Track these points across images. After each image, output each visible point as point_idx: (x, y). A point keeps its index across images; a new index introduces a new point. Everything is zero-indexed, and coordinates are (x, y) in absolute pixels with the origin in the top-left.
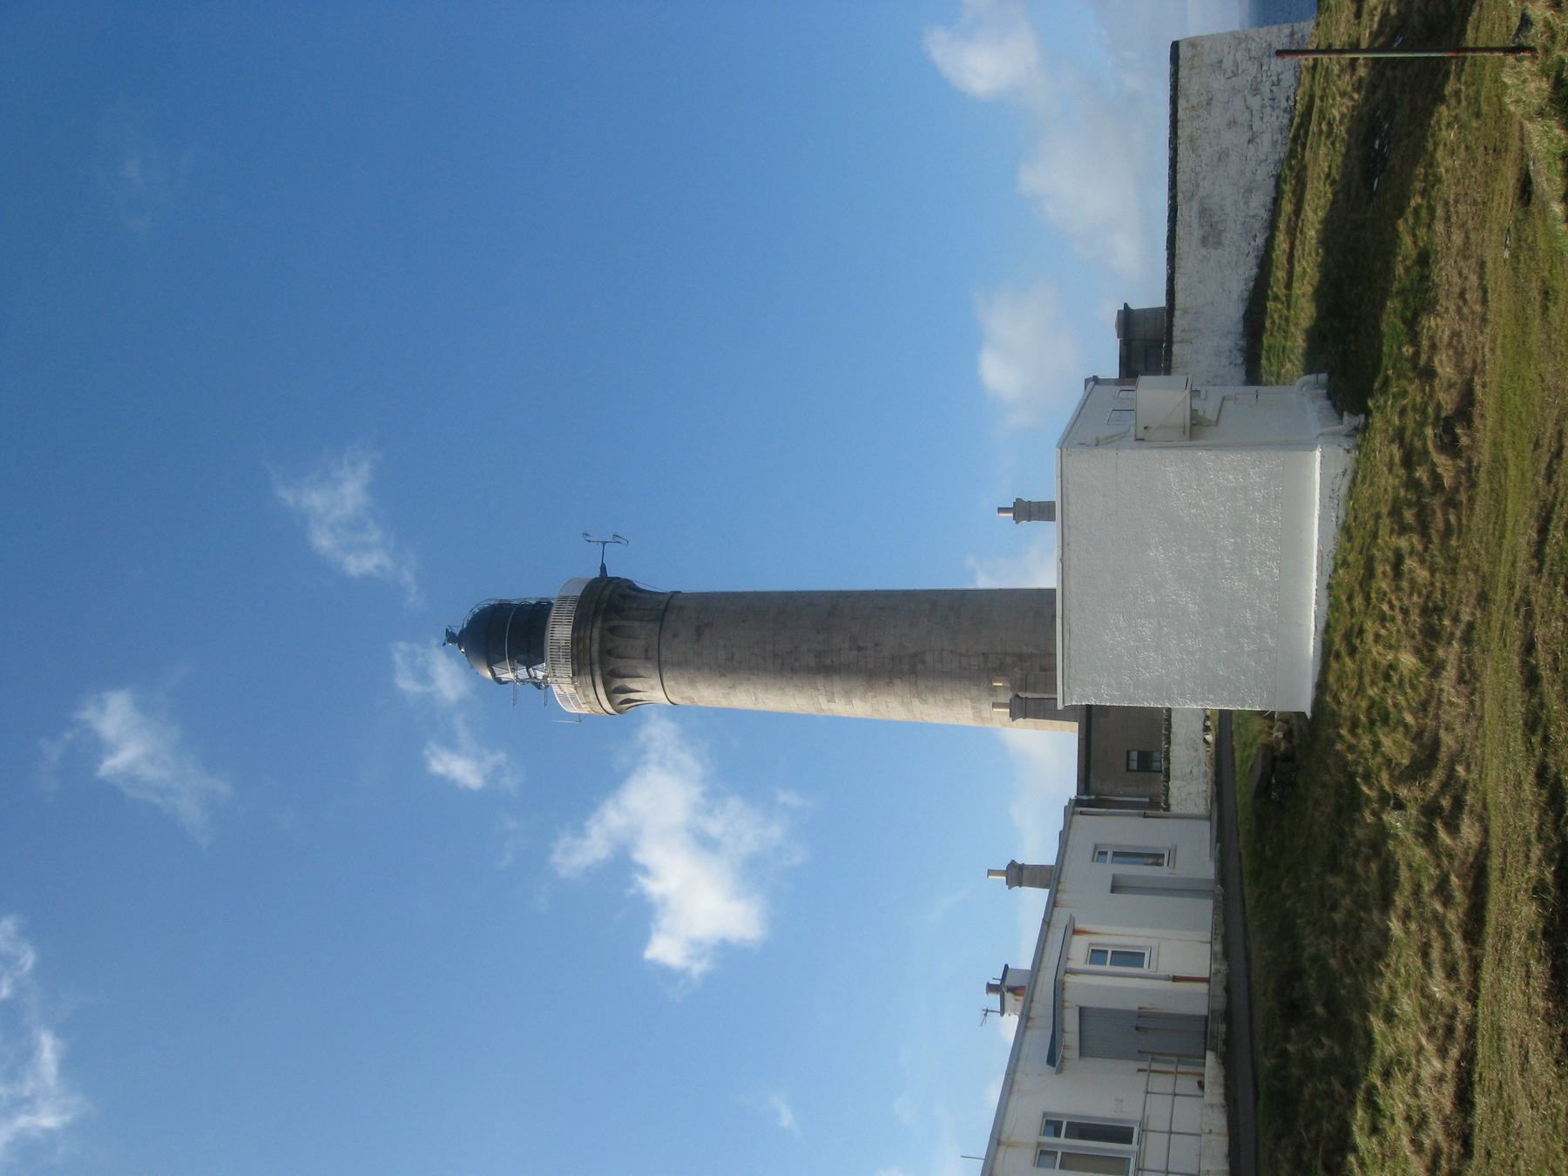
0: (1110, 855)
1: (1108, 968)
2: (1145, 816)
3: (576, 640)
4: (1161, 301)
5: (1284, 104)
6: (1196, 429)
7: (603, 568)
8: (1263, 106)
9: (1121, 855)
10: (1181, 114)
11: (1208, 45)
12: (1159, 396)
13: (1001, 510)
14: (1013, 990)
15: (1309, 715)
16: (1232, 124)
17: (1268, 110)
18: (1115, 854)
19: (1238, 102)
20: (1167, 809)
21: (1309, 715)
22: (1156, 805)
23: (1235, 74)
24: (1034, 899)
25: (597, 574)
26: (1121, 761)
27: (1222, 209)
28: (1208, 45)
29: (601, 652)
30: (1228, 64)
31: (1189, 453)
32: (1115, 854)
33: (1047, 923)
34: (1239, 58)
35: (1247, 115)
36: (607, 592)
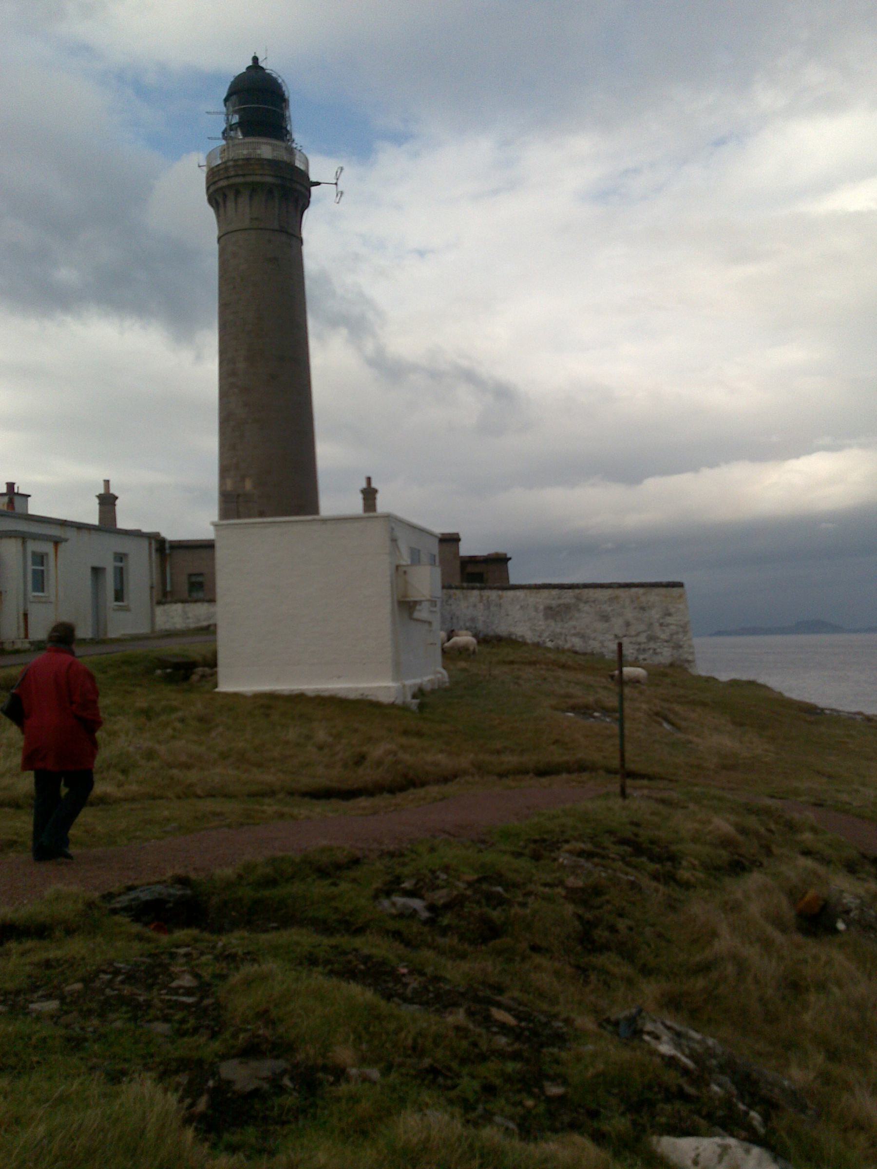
0: (119, 564)
1: (30, 567)
2: (152, 588)
3: (262, 162)
4: (513, 581)
5: (641, 657)
6: (406, 606)
7: (318, 184)
8: (639, 644)
9: (120, 573)
10: (634, 590)
11: (681, 606)
12: (426, 581)
13: (369, 480)
14: (11, 503)
15: (217, 690)
16: (628, 624)
17: (637, 647)
18: (121, 568)
19: (642, 627)
20: (159, 603)
21: (217, 690)
22: (164, 595)
23: (661, 625)
24: (91, 515)
25: (313, 178)
26: (182, 568)
27: (571, 618)
28: (681, 606)
29: (221, 188)
30: (669, 620)
31: (389, 600)
32: (121, 568)
33: (63, 524)
34: (672, 627)
35: (633, 633)
36: (298, 187)
